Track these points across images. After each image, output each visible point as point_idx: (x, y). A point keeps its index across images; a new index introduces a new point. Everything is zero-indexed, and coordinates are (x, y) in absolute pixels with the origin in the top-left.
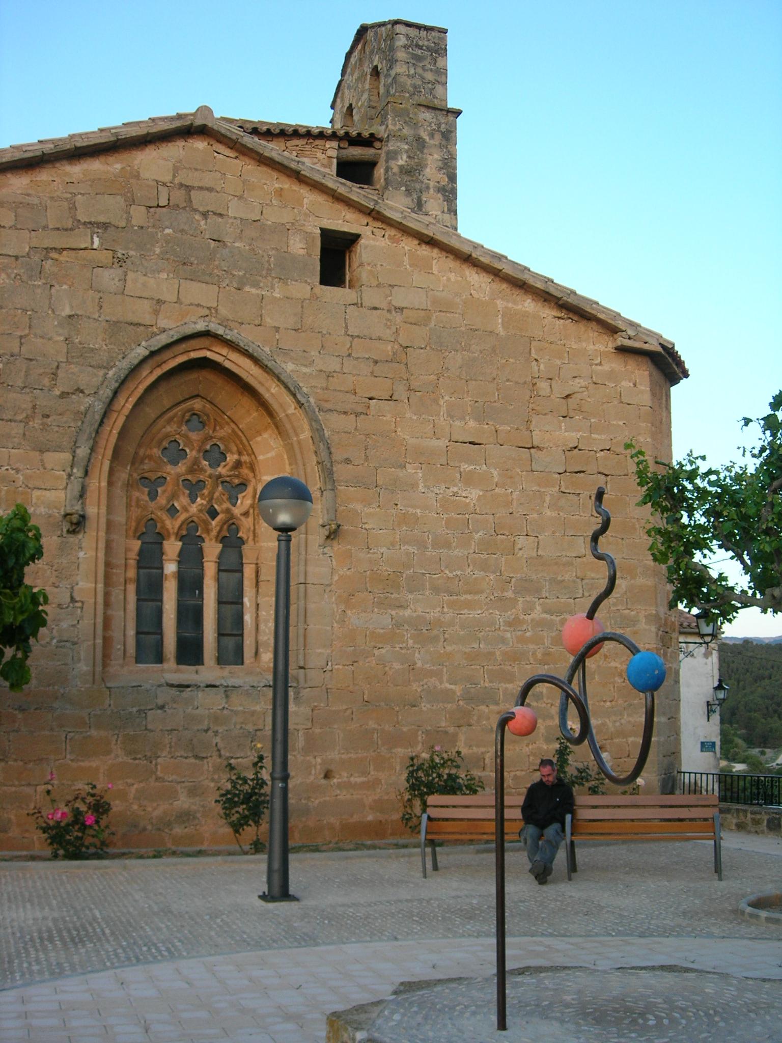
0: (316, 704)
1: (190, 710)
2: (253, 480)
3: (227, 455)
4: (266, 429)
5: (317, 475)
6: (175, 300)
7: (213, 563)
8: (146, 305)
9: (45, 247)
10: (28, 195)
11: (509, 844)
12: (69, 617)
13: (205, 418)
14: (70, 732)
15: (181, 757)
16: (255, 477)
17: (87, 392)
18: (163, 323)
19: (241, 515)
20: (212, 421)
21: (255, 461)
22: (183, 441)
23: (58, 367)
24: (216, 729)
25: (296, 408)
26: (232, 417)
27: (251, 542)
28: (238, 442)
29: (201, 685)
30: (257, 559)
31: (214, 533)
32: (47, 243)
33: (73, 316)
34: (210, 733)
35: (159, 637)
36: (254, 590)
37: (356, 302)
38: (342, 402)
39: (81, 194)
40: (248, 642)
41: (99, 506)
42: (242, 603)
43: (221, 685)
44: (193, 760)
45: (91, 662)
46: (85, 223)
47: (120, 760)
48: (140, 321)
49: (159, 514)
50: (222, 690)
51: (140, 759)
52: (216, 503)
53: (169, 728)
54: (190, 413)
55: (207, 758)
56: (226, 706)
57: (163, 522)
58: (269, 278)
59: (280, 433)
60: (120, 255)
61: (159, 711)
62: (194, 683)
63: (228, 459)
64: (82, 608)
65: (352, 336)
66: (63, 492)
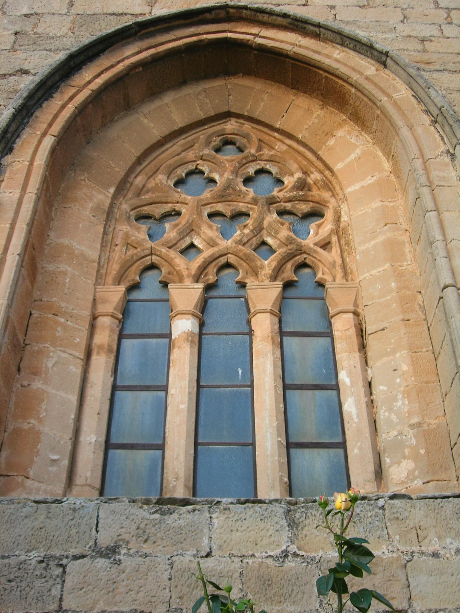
1: (188, 558)
2: (333, 200)
4: (340, 125)
5: (437, 136)
7: (268, 315)
19: (316, 244)
28: (300, 158)
30: (356, 305)
36: (357, 355)
40: (356, 451)
42: (336, 387)
48: (126, 12)
52: (269, 234)
56: (293, 548)
57: (169, 262)
61: (101, 562)
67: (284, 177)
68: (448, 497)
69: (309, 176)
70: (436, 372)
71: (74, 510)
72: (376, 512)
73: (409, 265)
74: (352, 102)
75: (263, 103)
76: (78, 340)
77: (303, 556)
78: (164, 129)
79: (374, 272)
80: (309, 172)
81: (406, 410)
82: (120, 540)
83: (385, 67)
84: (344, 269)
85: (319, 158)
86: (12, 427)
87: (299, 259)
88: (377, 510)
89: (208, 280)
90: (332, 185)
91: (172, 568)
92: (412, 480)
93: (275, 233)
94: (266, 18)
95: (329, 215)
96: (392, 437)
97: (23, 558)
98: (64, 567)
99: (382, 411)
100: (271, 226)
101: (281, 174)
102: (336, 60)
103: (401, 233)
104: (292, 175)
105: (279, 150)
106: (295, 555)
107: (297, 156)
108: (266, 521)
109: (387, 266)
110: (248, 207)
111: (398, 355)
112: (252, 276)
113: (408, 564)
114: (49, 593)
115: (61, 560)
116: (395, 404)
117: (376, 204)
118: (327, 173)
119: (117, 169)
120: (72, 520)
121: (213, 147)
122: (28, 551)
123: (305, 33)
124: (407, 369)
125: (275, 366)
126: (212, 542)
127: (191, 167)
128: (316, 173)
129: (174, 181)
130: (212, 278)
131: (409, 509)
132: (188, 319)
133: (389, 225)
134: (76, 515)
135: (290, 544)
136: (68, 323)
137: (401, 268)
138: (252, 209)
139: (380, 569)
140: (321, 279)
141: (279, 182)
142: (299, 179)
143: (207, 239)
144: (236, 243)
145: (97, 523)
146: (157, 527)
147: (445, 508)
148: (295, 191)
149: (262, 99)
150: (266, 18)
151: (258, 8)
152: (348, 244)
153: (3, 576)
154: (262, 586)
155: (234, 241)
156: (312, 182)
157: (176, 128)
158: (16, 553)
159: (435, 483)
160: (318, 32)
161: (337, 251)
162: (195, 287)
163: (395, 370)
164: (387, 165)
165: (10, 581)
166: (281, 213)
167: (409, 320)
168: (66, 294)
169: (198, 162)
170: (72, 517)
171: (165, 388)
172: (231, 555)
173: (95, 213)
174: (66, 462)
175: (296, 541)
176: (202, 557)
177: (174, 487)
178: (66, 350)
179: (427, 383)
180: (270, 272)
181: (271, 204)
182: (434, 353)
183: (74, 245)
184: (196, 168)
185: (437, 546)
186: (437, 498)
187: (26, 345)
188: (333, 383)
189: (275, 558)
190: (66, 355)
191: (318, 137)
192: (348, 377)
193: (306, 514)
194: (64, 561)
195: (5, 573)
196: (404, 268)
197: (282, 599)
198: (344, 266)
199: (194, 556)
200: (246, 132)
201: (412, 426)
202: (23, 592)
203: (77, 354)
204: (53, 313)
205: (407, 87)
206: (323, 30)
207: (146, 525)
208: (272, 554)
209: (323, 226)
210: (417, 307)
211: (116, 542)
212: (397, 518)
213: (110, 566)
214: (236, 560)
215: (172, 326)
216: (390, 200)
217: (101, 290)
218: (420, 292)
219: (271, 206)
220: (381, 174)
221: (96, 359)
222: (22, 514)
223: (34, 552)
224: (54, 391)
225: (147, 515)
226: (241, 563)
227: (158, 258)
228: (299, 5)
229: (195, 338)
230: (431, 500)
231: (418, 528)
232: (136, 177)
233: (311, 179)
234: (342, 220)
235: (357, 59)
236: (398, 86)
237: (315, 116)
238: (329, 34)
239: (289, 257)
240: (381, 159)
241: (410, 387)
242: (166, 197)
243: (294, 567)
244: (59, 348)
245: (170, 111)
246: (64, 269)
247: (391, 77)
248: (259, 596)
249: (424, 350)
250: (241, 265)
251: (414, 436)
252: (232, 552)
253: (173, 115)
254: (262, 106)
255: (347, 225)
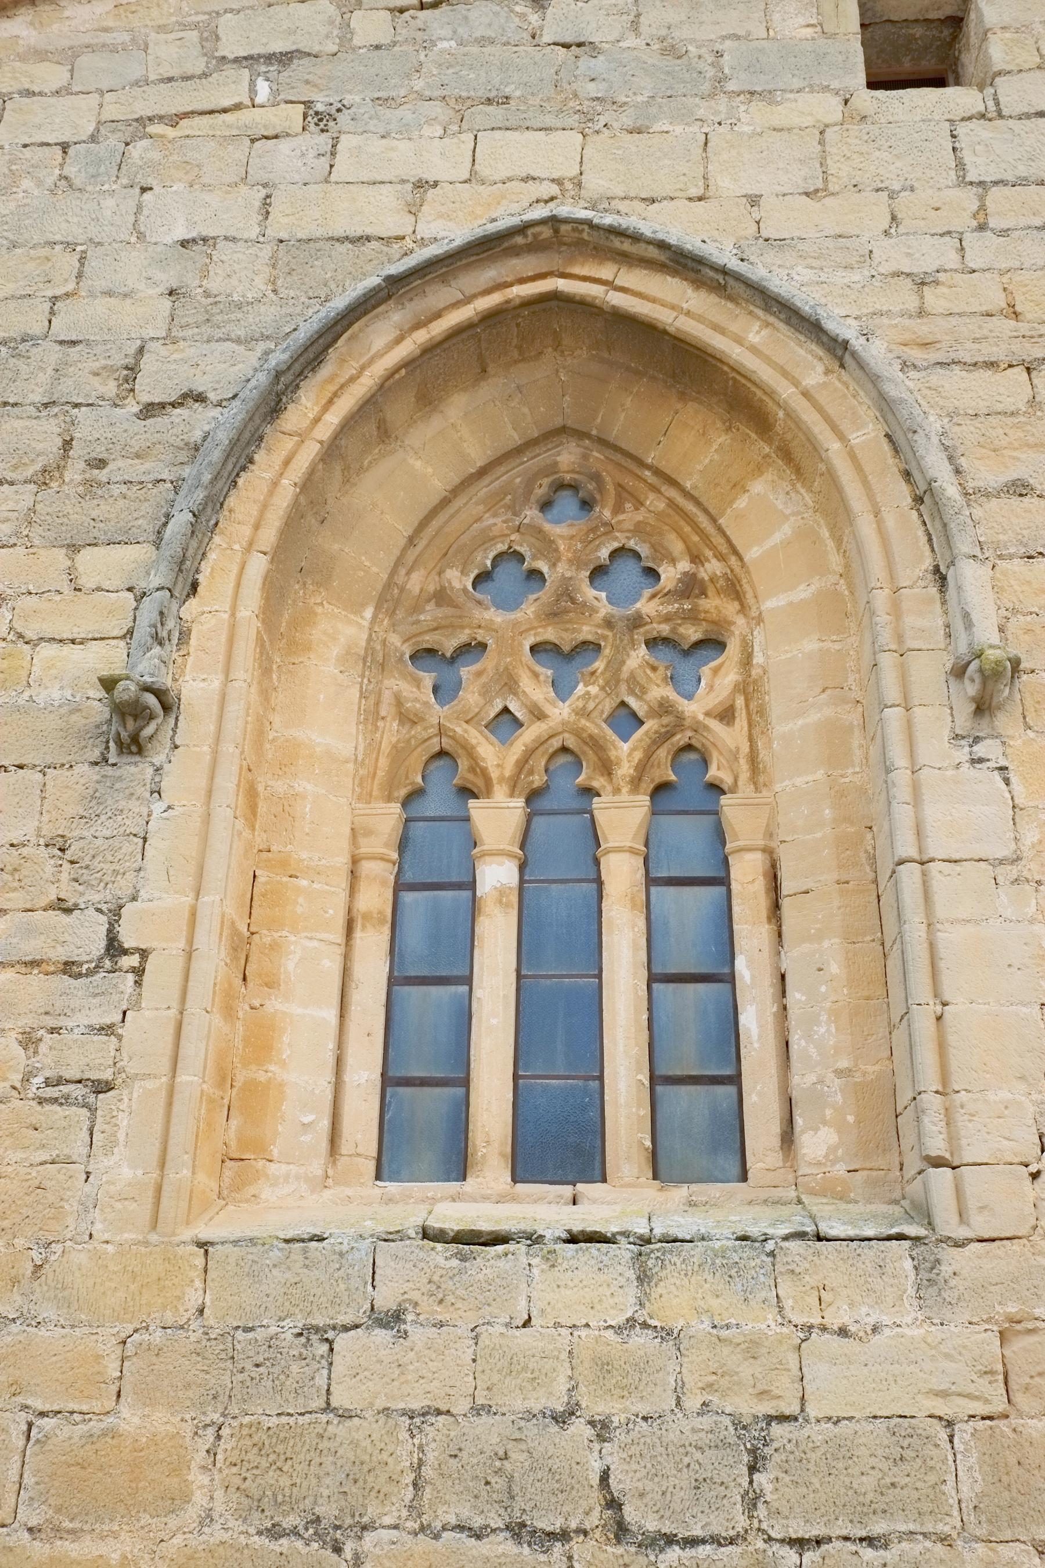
0: (1012, 1309)
2: (740, 621)
3: (660, 570)
4: (759, 470)
6: (466, 176)
8: (388, 197)
9: (136, 116)
10: (106, 30)
11: (392, 810)
12: (96, 1001)
13: (591, 486)
14: (42, 1414)
15: (460, 1528)
16: (743, 609)
17: (212, 396)
18: (425, 230)
19: (707, 714)
20: (610, 487)
21: (737, 570)
22: (531, 546)
23: (141, 350)
24: (600, 1408)
25: (827, 372)
26: (662, 465)
27: (745, 789)
28: (687, 529)
29: (548, 1234)
30: (770, 835)
31: (625, 770)
32: (143, 109)
33: (194, 240)
34: (580, 1428)
35: (460, 1091)
37: (981, 108)
38: (975, 340)
39: (232, 11)
40: (754, 1098)
41: (227, 671)
42: (730, 979)
43: (626, 1234)
44: (502, 1546)
45: (153, 1151)
46: (236, 60)
47: (216, 1534)
48: (369, 231)
49: (458, 730)
50: (624, 1250)
51: (295, 1532)
52: (631, 692)
53: (416, 1405)
54: (546, 482)
55: (564, 1536)
56: (642, 1316)
57: (470, 752)
58: (723, 99)
59: (798, 471)
60: (320, 107)
61: (382, 1335)
62: (523, 1226)
63: (663, 577)
64: (139, 972)
65: (981, 183)
66: (122, 644)
67: (659, 567)
68: (870, 1239)
69: (703, 565)
70: (883, 981)
71: (341, 1254)
72: (763, 1261)
73: (858, 773)
74: (778, 429)
75: (623, 414)
76: (331, 912)
77: (656, 1327)
78: (452, 474)
79: (799, 781)
80: (702, 559)
81: (831, 1043)
82: (404, 1301)
83: (842, 366)
84: (753, 765)
85: (720, 530)
86: (243, 1079)
87: (680, 739)
88: (765, 1258)
89: (533, 782)
90: (741, 586)
91: (476, 1344)
92: (834, 1163)
93: (640, 691)
94: (626, 246)
95: (733, 648)
96: (808, 1085)
97: (273, 1330)
98: (330, 1342)
99: (797, 1037)
100: (635, 679)
101: (654, 560)
102: (754, 350)
103: (847, 707)
104: (673, 561)
105: (652, 509)
106: (645, 1325)
107: (682, 523)
108: (606, 1271)
109: (820, 774)
110: (597, 633)
111: (826, 944)
112: (603, 775)
113: (803, 1345)
114: (312, 1383)
115: (326, 1332)
116: (815, 1028)
117: (811, 645)
118: (733, 560)
119: (375, 569)
120: (338, 1269)
121: (537, 502)
122: (280, 1319)
123: (699, 283)
124: (838, 971)
125: (635, 949)
126: (531, 1304)
127: (501, 547)
128: (714, 561)
129: (472, 576)
130: (538, 780)
131: (810, 1258)
132: (501, 864)
133: (829, 692)
134: (344, 1261)
135: (638, 1307)
136: (315, 885)
137: (843, 780)
138: (605, 638)
139: (764, 1351)
140: (716, 778)
141: (652, 574)
142: (685, 574)
143: (528, 704)
144: (577, 714)
145: (374, 1273)
146: (457, 1278)
147: (863, 1257)
148: (676, 601)
149: (622, 405)
150: (626, 246)
151: (610, 226)
152: (762, 712)
153: (248, 1357)
154: (599, 1373)
155: (573, 710)
156: (707, 578)
157: (473, 471)
158: (264, 1323)
159: (865, 1173)
160: (722, 282)
161: (742, 728)
162: (511, 805)
163: (820, 970)
164: (835, 561)
165: (257, 1366)
166: (651, 643)
167: (847, 882)
168: (307, 834)
169: (513, 537)
170: (338, 1266)
171: (468, 980)
172: (557, 1325)
173: (343, 665)
174: (325, 1124)
175: (647, 1304)
176: (518, 1327)
177: (484, 1156)
178: (313, 934)
179: (868, 998)
180: (631, 771)
181: (636, 627)
182: (883, 944)
183: (313, 738)
184: (510, 547)
185: (847, 1318)
186: (852, 1241)
187: (252, 934)
188: (726, 970)
189: (618, 1329)
190: (315, 944)
191: (718, 489)
192: (748, 967)
193: (662, 1261)
194: (330, 1335)
195: (251, 1354)
196: (847, 780)
197: (626, 1393)
198: (753, 758)
199: (507, 1325)
200: (594, 470)
201: (839, 1073)
202: (277, 1382)
203: (331, 937)
204: (290, 873)
205: (878, 414)
206: (731, 282)
207: (441, 1277)
208: (613, 1323)
209: (723, 670)
210: (863, 856)
211: (400, 1305)
212: (793, 1271)
213: (393, 1340)
214: (565, 1332)
215: (477, 872)
216: (834, 638)
217: (362, 812)
218: (870, 828)
219: (636, 631)
220: (824, 579)
221: (361, 938)
222: (268, 1262)
223: (288, 1321)
224: (300, 1011)
225: (441, 1261)
226: (570, 1337)
227: (451, 742)
228: (690, 199)
229: (511, 897)
230: (845, 1243)
231: (821, 1288)
232: (408, 573)
233: (706, 571)
234: (755, 662)
235: (792, 344)
236: (862, 410)
237: (715, 447)
238: (740, 289)
239: (664, 737)
240: (826, 546)
241: (840, 1004)
242: (460, 617)
243: (643, 1345)
244: (303, 935)
245: (461, 438)
246: (301, 790)
247: (851, 388)
248: (594, 1387)
249: (869, 938)
250: (584, 753)
251: (840, 1089)
252: (558, 1320)
253: (465, 445)
254: (622, 418)
255: (762, 673)
